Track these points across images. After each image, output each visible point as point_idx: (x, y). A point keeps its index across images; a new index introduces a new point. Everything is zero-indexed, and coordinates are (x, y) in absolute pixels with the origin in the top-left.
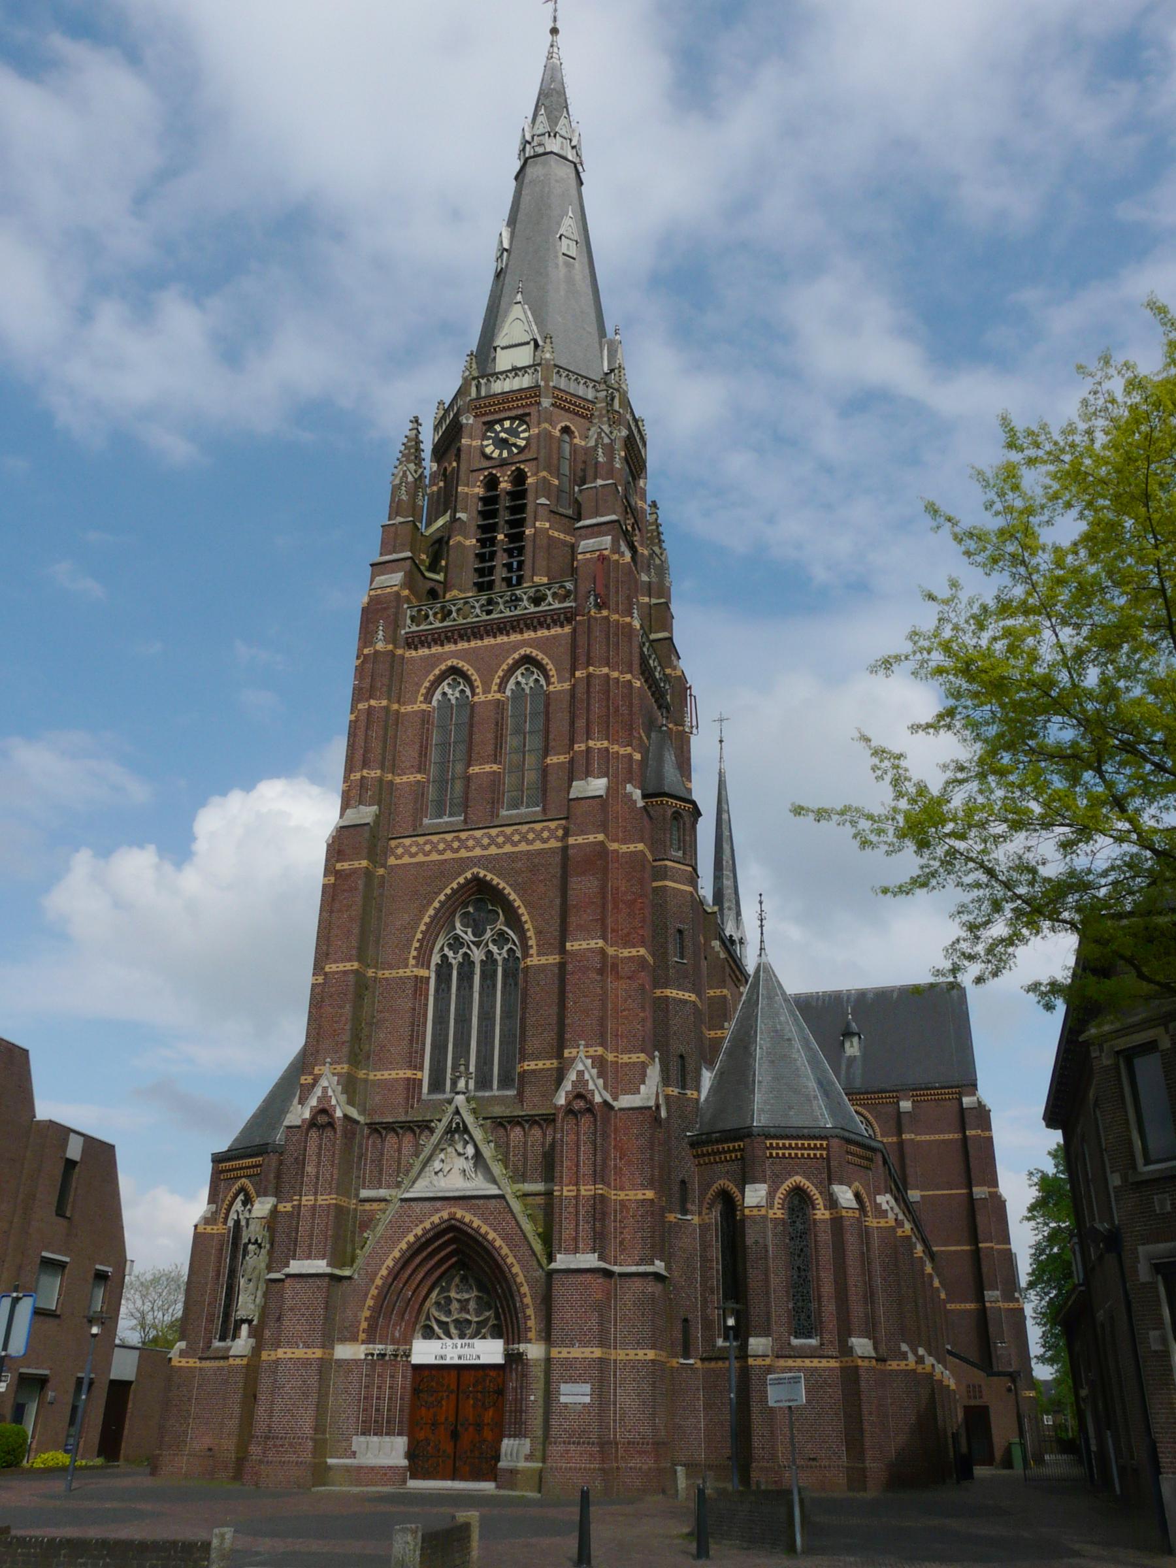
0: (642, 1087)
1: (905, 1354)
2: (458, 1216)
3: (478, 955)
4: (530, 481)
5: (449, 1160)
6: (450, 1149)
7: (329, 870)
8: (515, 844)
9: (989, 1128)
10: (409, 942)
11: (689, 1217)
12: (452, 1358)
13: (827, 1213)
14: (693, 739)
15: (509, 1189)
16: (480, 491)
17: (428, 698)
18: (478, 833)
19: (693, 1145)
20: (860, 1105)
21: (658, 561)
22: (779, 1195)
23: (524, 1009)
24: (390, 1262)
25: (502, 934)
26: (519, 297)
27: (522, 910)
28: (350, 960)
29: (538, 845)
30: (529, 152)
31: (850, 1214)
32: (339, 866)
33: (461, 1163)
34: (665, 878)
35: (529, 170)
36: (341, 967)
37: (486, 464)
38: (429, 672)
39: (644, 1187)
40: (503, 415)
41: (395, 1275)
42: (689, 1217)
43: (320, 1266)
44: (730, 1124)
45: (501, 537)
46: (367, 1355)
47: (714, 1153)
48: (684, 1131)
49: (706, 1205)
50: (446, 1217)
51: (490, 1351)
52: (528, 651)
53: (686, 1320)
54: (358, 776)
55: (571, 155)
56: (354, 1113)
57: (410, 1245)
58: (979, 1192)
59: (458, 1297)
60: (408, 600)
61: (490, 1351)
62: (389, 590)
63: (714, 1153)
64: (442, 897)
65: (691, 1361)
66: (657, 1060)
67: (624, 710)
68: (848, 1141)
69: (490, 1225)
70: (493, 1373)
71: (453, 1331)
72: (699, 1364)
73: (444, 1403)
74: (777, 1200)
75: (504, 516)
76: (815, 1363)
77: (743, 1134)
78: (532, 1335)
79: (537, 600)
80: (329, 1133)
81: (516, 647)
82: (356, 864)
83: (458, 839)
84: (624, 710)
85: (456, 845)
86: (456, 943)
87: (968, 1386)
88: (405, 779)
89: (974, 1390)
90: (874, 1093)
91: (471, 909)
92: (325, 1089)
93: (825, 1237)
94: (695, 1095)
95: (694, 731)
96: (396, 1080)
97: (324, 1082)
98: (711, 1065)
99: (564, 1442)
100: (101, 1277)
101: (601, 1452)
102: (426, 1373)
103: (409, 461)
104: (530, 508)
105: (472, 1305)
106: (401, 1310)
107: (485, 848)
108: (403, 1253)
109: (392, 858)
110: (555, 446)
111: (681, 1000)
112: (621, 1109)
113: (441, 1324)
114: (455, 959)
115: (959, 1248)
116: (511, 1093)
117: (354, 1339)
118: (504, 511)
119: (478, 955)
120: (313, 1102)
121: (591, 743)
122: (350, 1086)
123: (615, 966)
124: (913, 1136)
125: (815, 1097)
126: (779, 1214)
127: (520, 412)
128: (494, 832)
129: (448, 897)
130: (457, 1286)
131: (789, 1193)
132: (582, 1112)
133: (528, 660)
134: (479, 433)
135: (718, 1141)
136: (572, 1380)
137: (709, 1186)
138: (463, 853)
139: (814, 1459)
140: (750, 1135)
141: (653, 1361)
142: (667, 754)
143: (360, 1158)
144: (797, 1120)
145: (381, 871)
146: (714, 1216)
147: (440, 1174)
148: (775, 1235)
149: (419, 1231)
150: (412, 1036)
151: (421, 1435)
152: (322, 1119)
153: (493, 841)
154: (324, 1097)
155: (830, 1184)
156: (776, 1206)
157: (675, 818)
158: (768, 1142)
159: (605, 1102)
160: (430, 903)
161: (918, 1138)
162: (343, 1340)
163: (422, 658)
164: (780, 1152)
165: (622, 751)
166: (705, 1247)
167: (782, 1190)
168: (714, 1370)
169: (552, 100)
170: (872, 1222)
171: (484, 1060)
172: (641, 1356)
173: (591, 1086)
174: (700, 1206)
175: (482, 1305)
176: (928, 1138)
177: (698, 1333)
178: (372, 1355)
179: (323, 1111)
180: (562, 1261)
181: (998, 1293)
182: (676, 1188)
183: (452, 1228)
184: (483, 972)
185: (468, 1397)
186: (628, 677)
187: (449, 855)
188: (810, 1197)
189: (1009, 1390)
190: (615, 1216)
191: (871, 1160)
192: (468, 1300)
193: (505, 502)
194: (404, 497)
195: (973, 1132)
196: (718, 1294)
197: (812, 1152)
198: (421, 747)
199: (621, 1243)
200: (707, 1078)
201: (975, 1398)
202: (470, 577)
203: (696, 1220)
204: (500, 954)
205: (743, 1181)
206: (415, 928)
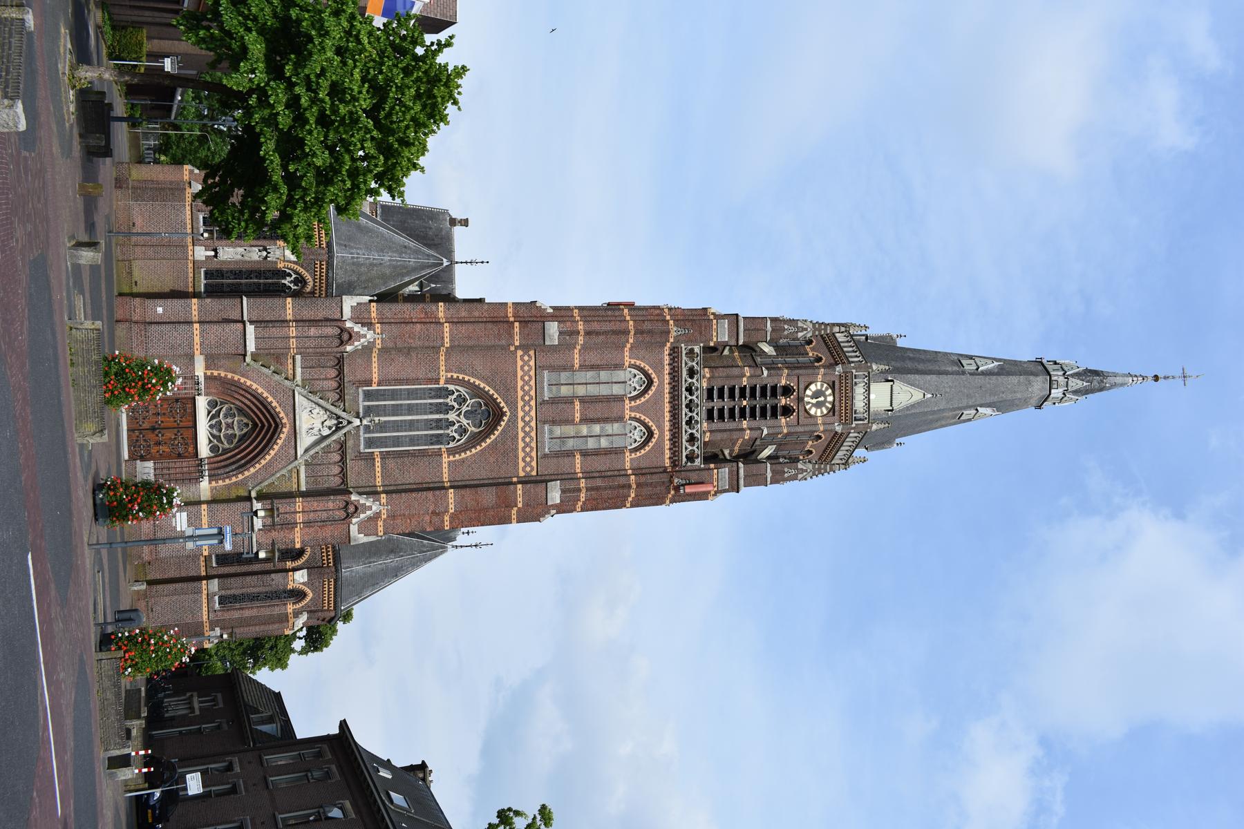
3: (452, 416)
15: (300, 461)
24: (255, 386)
25: (465, 431)
33: (318, 425)
41: (247, 390)
43: (251, 347)
51: (204, 451)
52: (656, 432)
64: (492, 392)
70: (191, 424)
71: (214, 422)
76: (205, 609)
80: (337, 342)
86: (461, 400)
88: (577, 356)
92: (365, 336)
93: (277, 611)
105: (230, 432)
106: (228, 393)
107: (523, 419)
108: (261, 395)
114: (450, 400)
117: (207, 368)
119: (452, 416)
122: (368, 349)
132: (340, 338)
138: (520, 403)
152: (345, 337)
154: (360, 336)
162: (206, 360)
173: (356, 343)
175: (230, 438)
179: (351, 336)
180: (250, 329)
187: (520, 393)
204: (452, 431)
206: (473, 375)
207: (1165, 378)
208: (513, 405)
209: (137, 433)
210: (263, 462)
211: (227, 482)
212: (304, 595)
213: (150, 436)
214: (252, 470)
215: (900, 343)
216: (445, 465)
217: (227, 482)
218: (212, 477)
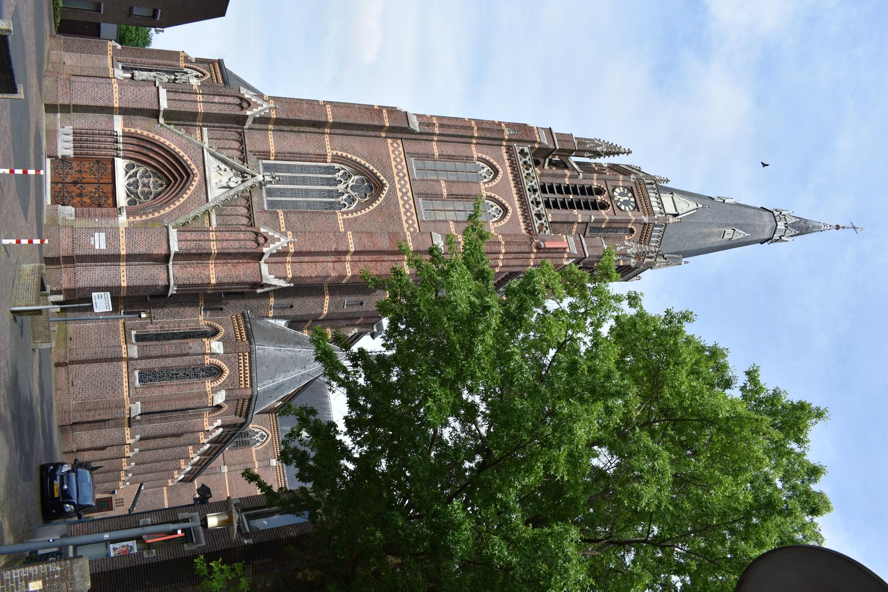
3: (341, 187)
4: (603, 211)
7: (381, 108)
8: (404, 206)
10: (346, 151)
16: (595, 184)
17: (481, 159)
18: (408, 186)
22: (218, 361)
23: (313, 212)
24: (167, 143)
25: (354, 200)
26: (700, 206)
30: (776, 213)
32: (384, 111)
35: (767, 213)
36: (329, 113)
37: (610, 189)
39: (217, 278)
45: (571, 197)
47: (239, 325)
50: (195, 172)
52: (510, 211)
54: (435, 122)
55: (776, 237)
61: (122, 199)
63: (239, 325)
68: (250, 400)
69: (191, 195)
70: (110, 181)
71: (132, 180)
74: (215, 360)
75: (582, 198)
76: (126, 384)
78: (131, 219)
79: (539, 216)
81: (512, 205)
82: (386, 120)
85: (401, 175)
91: (366, 184)
93: (196, 389)
96: (269, 145)
97: (265, 106)
100: (154, 15)
103: (607, 147)
104: (587, 212)
105: (146, 189)
113: (135, 174)
114: (338, 176)
116: (266, 207)
117: (125, 126)
118: (587, 198)
119: (341, 187)
120: (254, 100)
126: (207, 362)
127: (640, 206)
128: (410, 194)
129: (372, 171)
134: (626, 184)
135: (246, 327)
136: (107, 239)
137: (220, 324)
138: (396, 179)
144: (261, 370)
149: (186, 158)
151: (74, 164)
153: (404, 194)
159: (263, 254)
167: (221, 363)
168: (118, 329)
169: (803, 228)
171: (282, 192)
173: (272, 246)
184: (332, 191)
187: (395, 171)
194: (588, 146)
202: (548, 181)
207: (844, 228)
209: (60, 185)
210: (177, 204)
211: (144, 218)
212: (220, 371)
213: (72, 188)
214: (167, 210)
216: (340, 222)
217: (144, 218)
218: (129, 215)
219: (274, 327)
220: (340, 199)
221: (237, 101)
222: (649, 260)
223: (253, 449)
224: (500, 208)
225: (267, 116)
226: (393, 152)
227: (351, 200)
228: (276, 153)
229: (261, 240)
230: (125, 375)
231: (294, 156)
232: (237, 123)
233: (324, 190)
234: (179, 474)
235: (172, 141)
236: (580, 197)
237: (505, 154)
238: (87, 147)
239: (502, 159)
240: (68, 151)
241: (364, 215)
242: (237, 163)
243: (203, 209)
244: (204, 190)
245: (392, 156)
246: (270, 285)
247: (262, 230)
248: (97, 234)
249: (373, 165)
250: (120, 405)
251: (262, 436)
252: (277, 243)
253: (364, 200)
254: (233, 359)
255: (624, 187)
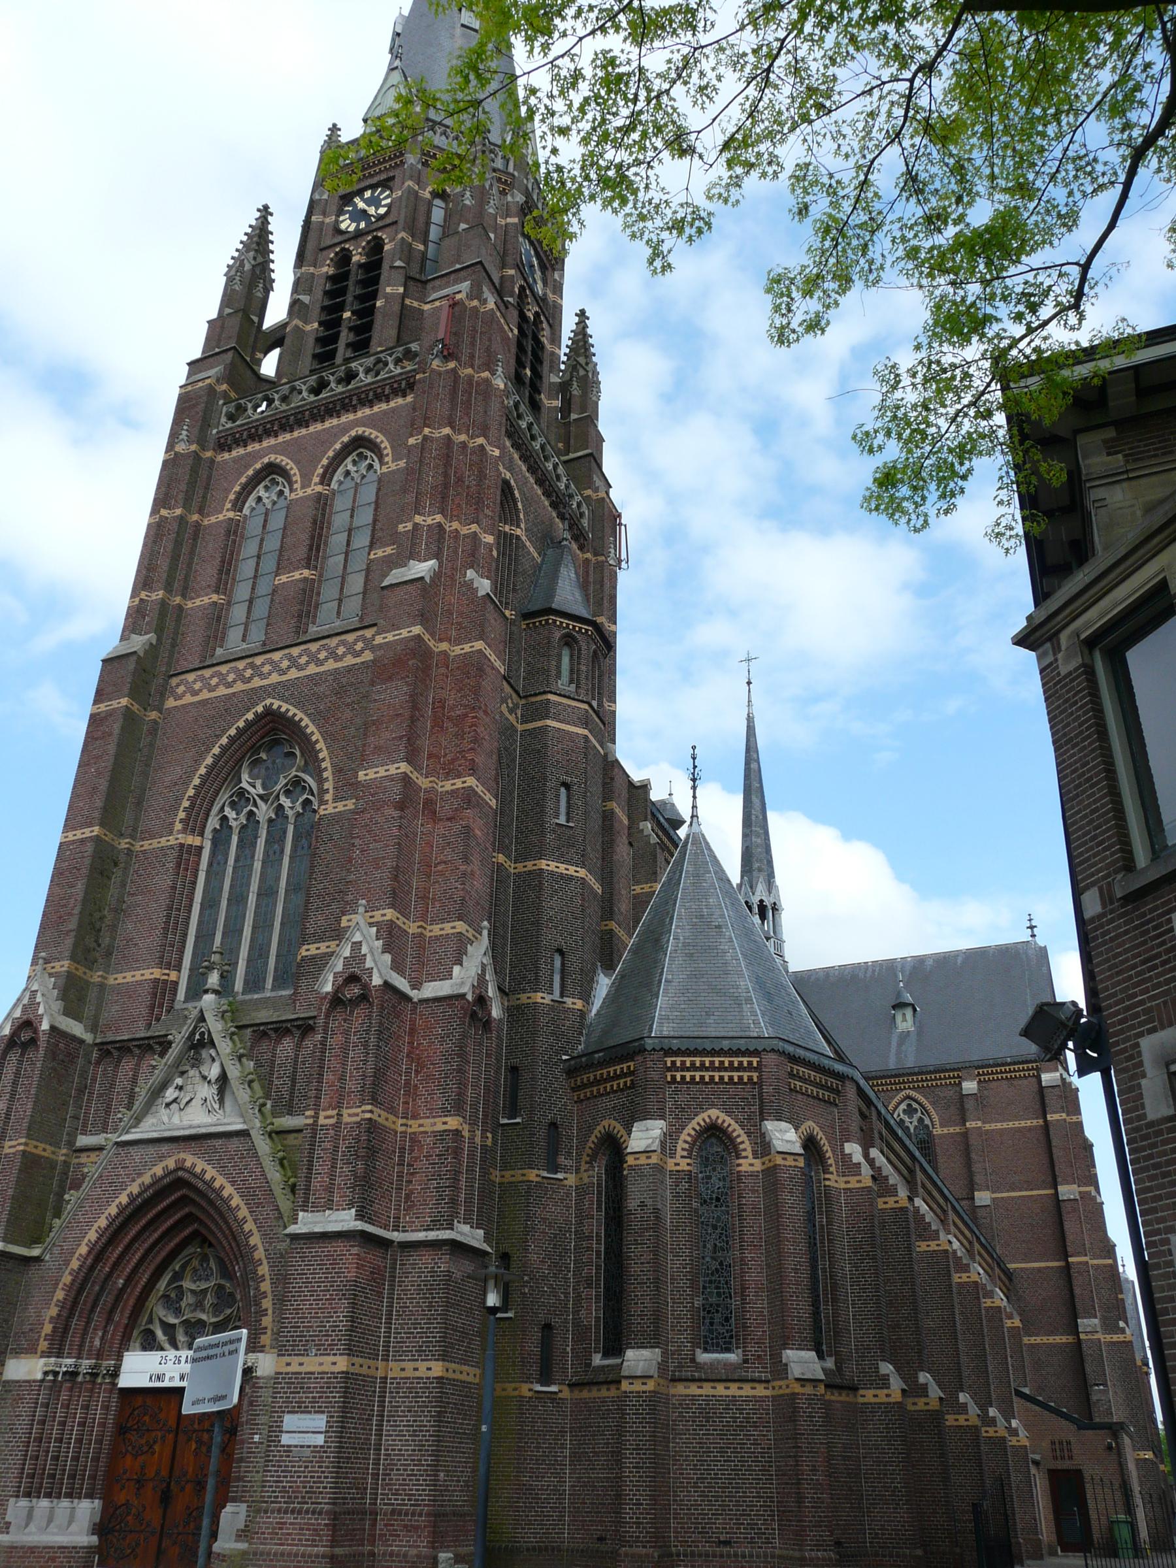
0: (456, 969)
1: (886, 1378)
2: (188, 1164)
3: (264, 812)
4: (386, 247)
5: (189, 1087)
6: (192, 1073)
9: (1077, 1110)
10: (178, 801)
11: (560, 1176)
12: (171, 1379)
13: (757, 1162)
14: (621, 576)
17: (238, 505)
18: (276, 656)
19: (571, 1072)
20: (914, 1089)
21: (582, 372)
22: (684, 1136)
24: (92, 1236)
27: (321, 745)
28: (90, 825)
29: (349, 660)
31: (790, 1162)
34: (547, 717)
38: (241, 474)
40: (362, 185)
41: (98, 1254)
42: (560, 1176)
44: (624, 1035)
46: (46, 1373)
47: (597, 1082)
48: (557, 1053)
49: (585, 1158)
53: (547, 1327)
56: (76, 1028)
57: (122, 1209)
58: (1067, 1191)
59: (193, 1287)
60: (225, 395)
62: (201, 384)
63: (597, 1082)
65: (553, 1388)
66: (485, 932)
67: (470, 480)
68: (794, 1059)
69: (227, 1176)
71: (181, 1338)
72: (566, 1393)
73: (157, 1448)
74: (681, 1145)
75: (353, 290)
76: (734, 1390)
77: (632, 1050)
81: (344, 429)
83: (252, 666)
84: (470, 480)
86: (241, 798)
87: (1053, 1443)
89: (1061, 1448)
90: (930, 1072)
91: (264, 756)
93: (753, 1198)
94: (579, 1004)
95: (624, 565)
98: (609, 967)
99: (279, 1511)
101: (334, 1528)
102: (139, 1400)
105: (209, 1300)
107: (283, 672)
109: (171, 699)
110: (422, 209)
111: (562, 876)
112: (422, 1001)
113: (169, 1329)
115: (1043, 1264)
116: (287, 992)
117: (31, 1350)
119: (264, 812)
121: (418, 519)
123: (429, 804)
124: (979, 1124)
125: (749, 1000)
126: (684, 1165)
127: (383, 176)
129: (232, 740)
130: (195, 1270)
131: (700, 1134)
133: (360, 442)
134: (334, 208)
135: (603, 1064)
136: (301, 1409)
137: (590, 1130)
138: (257, 682)
139: (727, 1543)
140: (642, 1050)
141: (439, 1379)
142: (563, 571)
143: (81, 1091)
145: (154, 715)
146: (596, 1173)
147: (174, 1106)
148: (677, 1196)
149: (135, 1189)
150: (167, 923)
151: (121, 1498)
155: (762, 1120)
156: (680, 1153)
157: (567, 644)
158: (669, 1060)
160: (208, 750)
161: (987, 1127)
162: (18, 1352)
163: (235, 460)
164: (688, 1075)
165: (464, 531)
166: (581, 1217)
167: (689, 1130)
170: (835, 1180)
171: (259, 952)
172: (422, 1372)
174: (578, 1162)
176: (999, 1126)
177: (567, 1346)
178: (56, 1374)
181: (1096, 1321)
182: (542, 1133)
183: (179, 1183)
185: (189, 1440)
186: (481, 440)
187: (239, 687)
188: (732, 1140)
189: (1110, 1448)
190: (402, 1157)
191: (837, 1092)
192: (204, 1292)
193: (355, 275)
195: (1056, 1117)
196: (598, 1286)
197: (736, 1075)
198: (223, 562)
199: (408, 1197)
200: (604, 984)
201: (1063, 1458)
203: (571, 1180)
205: (632, 1116)
208: (255, 695)
210: (244, 1212)
215: (406, 13)
219: (613, 998)
220: (290, 813)
221: (13, 1057)
222: (511, 164)
223: (938, 1131)
224: (354, 456)
225: (62, 981)
226: (195, 693)
227: (296, 785)
228: (160, 965)
229: (355, 990)
230: (707, 1389)
231: (175, 923)
232: (71, 1057)
233: (266, 853)
234: (990, 1294)
235: (89, 1224)
236: (349, 298)
237: (234, 453)
238: (76, 1459)
239: (241, 458)
240: (37, 1513)
241: (331, 753)
242: (161, 1064)
243: (263, 1145)
244: (218, 1143)
245: (205, 695)
246: (481, 978)
247: (328, 988)
248: (286, 1439)
249: (219, 737)
250: (787, 1407)
251: (910, 1111)
252: (39, 999)
253: (299, 761)
254: (682, 1098)
255: (340, 212)
